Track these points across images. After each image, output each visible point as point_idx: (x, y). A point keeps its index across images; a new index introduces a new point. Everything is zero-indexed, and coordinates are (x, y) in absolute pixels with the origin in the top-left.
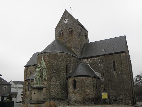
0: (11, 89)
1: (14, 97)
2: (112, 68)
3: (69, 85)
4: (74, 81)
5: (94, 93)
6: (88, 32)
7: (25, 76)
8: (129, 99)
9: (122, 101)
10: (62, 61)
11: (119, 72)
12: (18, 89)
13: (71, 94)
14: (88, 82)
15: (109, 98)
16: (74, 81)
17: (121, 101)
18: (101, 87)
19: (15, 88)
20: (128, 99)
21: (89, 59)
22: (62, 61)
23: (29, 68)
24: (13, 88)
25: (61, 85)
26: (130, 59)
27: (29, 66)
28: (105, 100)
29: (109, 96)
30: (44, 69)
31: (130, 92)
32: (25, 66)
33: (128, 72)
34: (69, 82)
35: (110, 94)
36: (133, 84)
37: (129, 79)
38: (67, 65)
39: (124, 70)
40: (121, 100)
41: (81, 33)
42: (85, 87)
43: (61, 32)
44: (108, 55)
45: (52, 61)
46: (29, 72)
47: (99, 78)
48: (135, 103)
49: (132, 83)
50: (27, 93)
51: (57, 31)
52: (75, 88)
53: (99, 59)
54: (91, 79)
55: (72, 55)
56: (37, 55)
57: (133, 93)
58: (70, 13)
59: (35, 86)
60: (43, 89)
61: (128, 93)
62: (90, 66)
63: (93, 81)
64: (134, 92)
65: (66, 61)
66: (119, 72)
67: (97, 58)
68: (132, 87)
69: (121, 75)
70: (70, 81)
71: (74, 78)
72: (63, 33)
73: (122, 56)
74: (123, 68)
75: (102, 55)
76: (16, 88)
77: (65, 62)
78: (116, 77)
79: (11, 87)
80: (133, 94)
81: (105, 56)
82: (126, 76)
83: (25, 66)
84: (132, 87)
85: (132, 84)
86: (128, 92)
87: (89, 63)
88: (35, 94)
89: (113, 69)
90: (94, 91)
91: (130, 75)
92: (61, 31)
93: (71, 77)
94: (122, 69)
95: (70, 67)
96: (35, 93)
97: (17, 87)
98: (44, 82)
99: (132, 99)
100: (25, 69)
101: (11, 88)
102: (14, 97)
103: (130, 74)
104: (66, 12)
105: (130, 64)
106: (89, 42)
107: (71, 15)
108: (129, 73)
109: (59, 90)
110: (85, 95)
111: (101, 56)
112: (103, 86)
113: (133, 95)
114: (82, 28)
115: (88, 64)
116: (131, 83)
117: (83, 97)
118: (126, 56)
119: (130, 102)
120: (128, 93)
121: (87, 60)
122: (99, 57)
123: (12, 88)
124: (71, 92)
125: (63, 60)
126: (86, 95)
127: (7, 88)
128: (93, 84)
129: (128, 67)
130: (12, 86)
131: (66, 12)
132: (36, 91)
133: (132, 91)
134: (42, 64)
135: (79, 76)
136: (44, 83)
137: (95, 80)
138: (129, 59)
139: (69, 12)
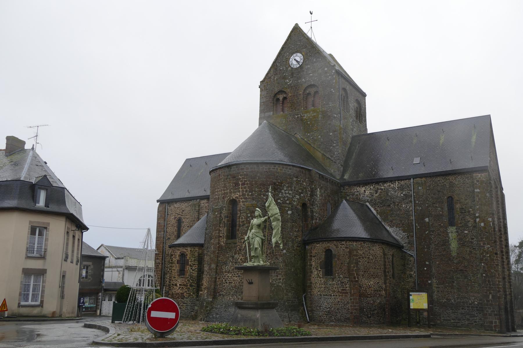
0: (105, 273)
1: (107, 299)
2: (444, 218)
3: (311, 265)
4: (328, 252)
5: (385, 290)
6: (364, 95)
7: (160, 232)
8: (495, 315)
9: (471, 319)
10: (290, 192)
11: (466, 232)
12: (126, 272)
13: (315, 291)
14: (369, 258)
15: (430, 310)
16: (328, 252)
17: (468, 320)
18: (405, 273)
19: (114, 269)
20: (490, 315)
21: (372, 187)
22: (290, 192)
23: (174, 209)
24: (111, 269)
25: (286, 265)
26: (502, 189)
27: (179, 201)
28: (419, 311)
29: (430, 301)
30: (274, 221)
31: (499, 291)
32: (158, 201)
33: (494, 231)
34: (311, 256)
35: (435, 297)
36: (509, 268)
37: (496, 254)
38: (304, 205)
39: (482, 224)
40: (467, 317)
41: (345, 99)
42: (361, 273)
43: (281, 97)
44: (433, 176)
45: (261, 191)
46: (172, 220)
47: (398, 247)
48: (510, 327)
49: (506, 266)
50: (176, 285)
51: (265, 93)
52: (331, 275)
53: (401, 188)
54: (377, 250)
55: (320, 175)
56: (210, 172)
57: (506, 295)
58: (309, 35)
59: (249, 264)
60: (270, 271)
61: (491, 297)
62: (372, 209)
63: (385, 254)
64: (510, 294)
65: (302, 193)
66: (466, 232)
67: (396, 185)
68: (504, 278)
69: (472, 239)
70: (314, 252)
71: (326, 245)
72: (285, 98)
73: (478, 181)
74: (478, 220)
75: (415, 177)
76: (120, 269)
77: (300, 195)
78: (454, 245)
79: (106, 266)
80: (505, 298)
81: (423, 179)
82: (488, 244)
83: (158, 201)
84: (504, 278)
85: (503, 268)
86: (490, 293)
87: (370, 199)
88: (251, 285)
89: (446, 219)
90: (386, 287)
91: (501, 241)
92: (281, 92)
93: (318, 242)
94: (475, 221)
95: (312, 212)
96: (251, 283)
97: (121, 267)
98: (236, 254)
99: (503, 313)
100: (161, 208)
101: (106, 270)
102: (107, 299)
103: (501, 237)
104: (296, 31)
105: (500, 206)
106: (369, 131)
107: (313, 39)
108: (498, 234)
109: (280, 279)
110: (360, 296)
111: (408, 178)
112: (412, 273)
113: (506, 303)
114: (348, 87)
115: (368, 204)
116: (503, 265)
117: (353, 303)
118: (490, 183)
119: (496, 322)
120: (491, 297)
121: (363, 189)
122: (403, 183)
123: (109, 267)
124: (318, 285)
125: (292, 191)
126: (362, 295)
127: (92, 267)
128: (385, 265)
129: (496, 217)
130: (107, 261)
131: (296, 31)
132: (255, 278)
133: (505, 291)
134: (269, 206)
135: (343, 240)
136: (236, 256)
137: (390, 252)
138: (499, 193)
139: (305, 29)
